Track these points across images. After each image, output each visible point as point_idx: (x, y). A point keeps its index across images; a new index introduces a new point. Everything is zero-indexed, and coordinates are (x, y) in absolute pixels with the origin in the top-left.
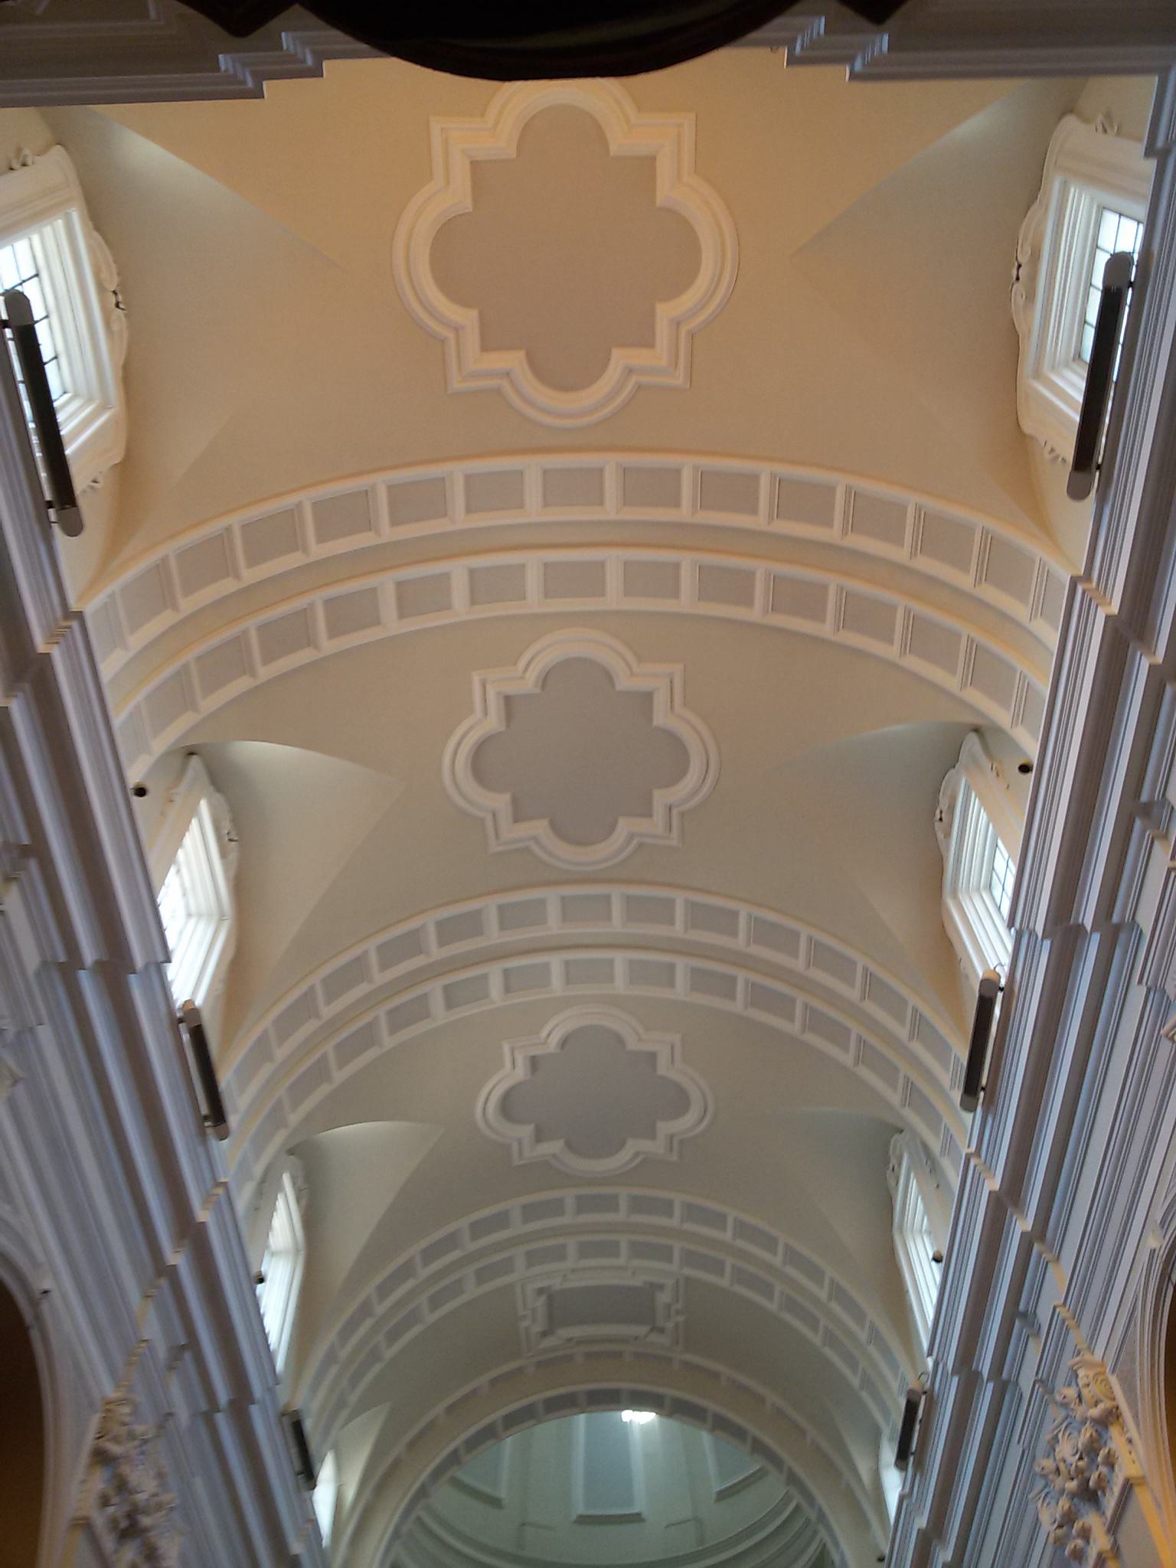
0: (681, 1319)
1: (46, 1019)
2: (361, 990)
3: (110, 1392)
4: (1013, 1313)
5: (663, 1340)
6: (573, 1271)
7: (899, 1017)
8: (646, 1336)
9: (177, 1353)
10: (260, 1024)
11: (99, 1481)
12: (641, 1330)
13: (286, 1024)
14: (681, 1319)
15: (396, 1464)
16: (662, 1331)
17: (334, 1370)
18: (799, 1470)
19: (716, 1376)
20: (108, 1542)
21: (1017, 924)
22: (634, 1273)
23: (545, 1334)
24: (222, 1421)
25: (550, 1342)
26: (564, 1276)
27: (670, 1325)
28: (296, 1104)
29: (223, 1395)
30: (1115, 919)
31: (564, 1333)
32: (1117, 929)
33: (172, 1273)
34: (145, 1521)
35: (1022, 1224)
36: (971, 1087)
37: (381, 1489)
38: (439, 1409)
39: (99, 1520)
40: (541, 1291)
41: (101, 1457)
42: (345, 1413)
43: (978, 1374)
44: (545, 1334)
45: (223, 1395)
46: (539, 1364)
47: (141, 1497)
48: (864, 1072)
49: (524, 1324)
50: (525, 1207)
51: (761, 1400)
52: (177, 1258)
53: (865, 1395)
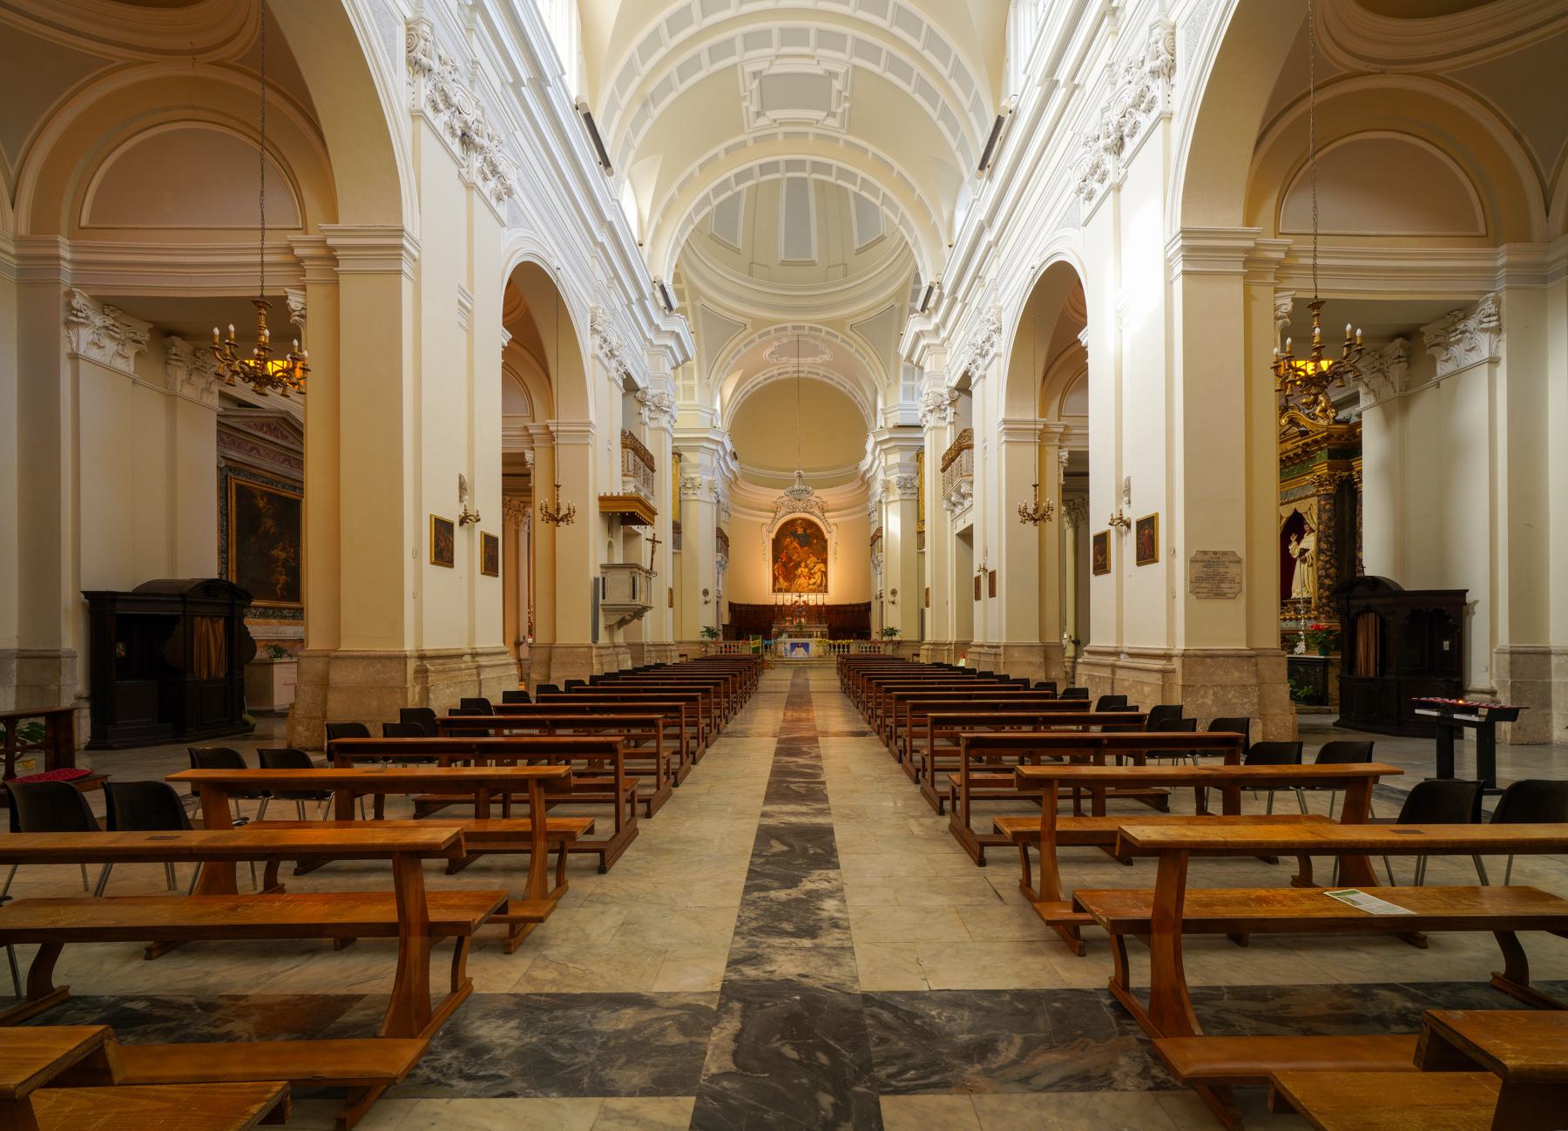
0: (847, 105)
1: (517, 127)
2: (662, 51)
3: (591, 305)
4: (976, 277)
5: (833, 122)
6: (777, 57)
7: (954, 135)
8: (824, 120)
9: (609, 279)
10: (608, 86)
11: (598, 340)
12: (821, 115)
13: (622, 83)
14: (847, 105)
15: (672, 199)
16: (834, 115)
17: (618, 114)
18: (908, 216)
19: (865, 151)
20: (493, 202)
21: (1028, 72)
22: (819, 61)
23: (758, 114)
24: (636, 308)
25: (762, 121)
26: (771, 61)
27: (840, 110)
28: (635, 135)
29: (634, 297)
30: (1076, 82)
31: (772, 114)
32: (1077, 86)
33: (602, 246)
34: (616, 353)
35: (989, 237)
36: (982, 167)
37: (664, 215)
38: (694, 166)
39: (601, 355)
40: (755, 75)
41: (594, 331)
42: (632, 153)
43: (957, 298)
44: (758, 114)
45: (634, 297)
46: (756, 139)
47: (470, 119)
48: (941, 124)
49: (745, 104)
50: (746, 36)
51: (892, 168)
52: (602, 237)
53: (958, 155)
